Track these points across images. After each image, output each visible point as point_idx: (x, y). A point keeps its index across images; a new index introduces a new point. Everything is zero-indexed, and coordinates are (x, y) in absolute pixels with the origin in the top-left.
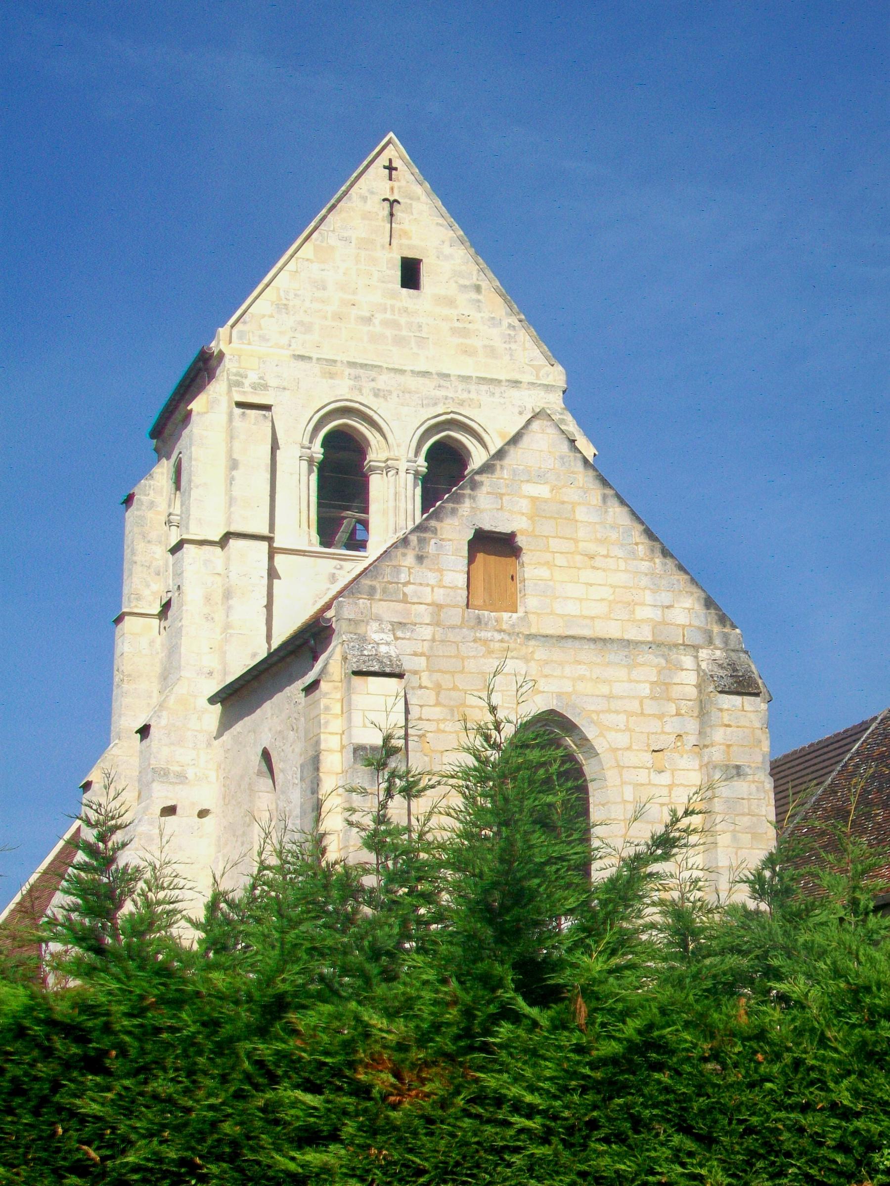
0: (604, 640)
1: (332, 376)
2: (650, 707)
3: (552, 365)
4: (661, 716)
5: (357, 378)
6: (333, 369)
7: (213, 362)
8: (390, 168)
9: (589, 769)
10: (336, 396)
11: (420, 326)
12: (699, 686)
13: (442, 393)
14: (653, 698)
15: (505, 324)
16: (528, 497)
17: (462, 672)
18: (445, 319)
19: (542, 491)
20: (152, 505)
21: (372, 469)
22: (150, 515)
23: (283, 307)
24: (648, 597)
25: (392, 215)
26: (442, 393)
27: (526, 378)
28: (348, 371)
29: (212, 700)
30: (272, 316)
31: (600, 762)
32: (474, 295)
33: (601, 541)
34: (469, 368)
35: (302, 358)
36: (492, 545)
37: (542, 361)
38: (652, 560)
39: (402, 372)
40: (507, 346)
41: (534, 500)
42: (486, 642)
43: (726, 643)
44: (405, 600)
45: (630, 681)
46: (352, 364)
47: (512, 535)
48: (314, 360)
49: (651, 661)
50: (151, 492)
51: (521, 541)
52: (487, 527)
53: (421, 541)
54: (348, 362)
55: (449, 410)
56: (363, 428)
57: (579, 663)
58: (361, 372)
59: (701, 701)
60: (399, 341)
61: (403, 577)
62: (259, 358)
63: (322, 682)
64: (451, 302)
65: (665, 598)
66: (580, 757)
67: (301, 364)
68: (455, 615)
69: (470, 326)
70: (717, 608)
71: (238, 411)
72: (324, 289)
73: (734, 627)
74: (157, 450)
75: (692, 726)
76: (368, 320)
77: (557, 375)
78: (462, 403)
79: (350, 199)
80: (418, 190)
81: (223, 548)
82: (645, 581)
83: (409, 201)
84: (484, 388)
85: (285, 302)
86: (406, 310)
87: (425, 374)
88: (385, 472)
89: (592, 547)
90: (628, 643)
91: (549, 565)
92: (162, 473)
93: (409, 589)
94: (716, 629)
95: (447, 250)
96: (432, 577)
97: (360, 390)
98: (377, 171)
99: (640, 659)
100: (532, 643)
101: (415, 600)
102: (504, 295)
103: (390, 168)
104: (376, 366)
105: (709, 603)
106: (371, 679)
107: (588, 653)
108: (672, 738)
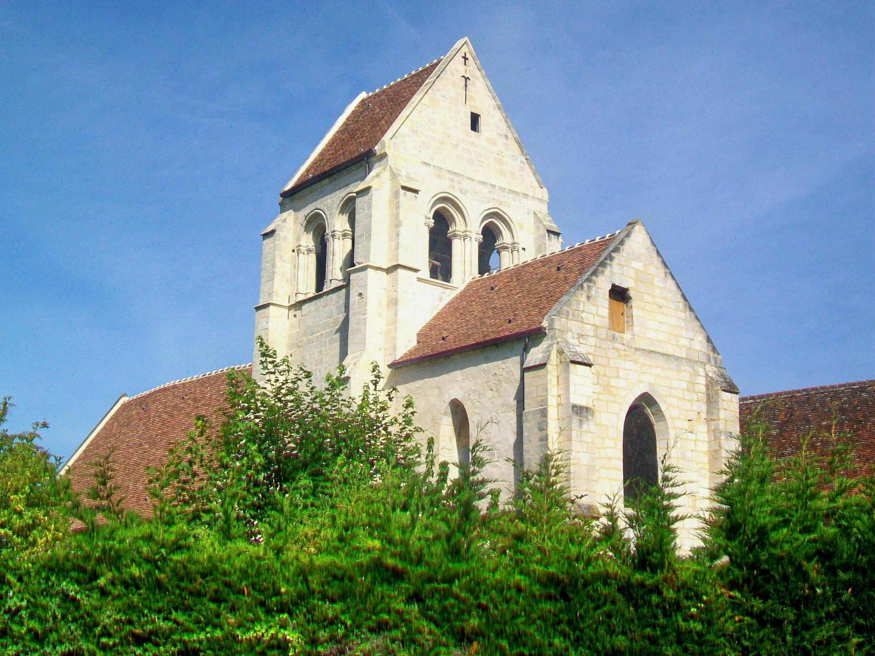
0: (667, 355)
2: (687, 396)
4: (691, 401)
7: (374, 159)
8: (465, 58)
9: (658, 427)
12: (707, 386)
13: (491, 196)
14: (688, 390)
17: (608, 366)
19: (638, 265)
20: (285, 238)
21: (455, 236)
23: (415, 131)
24: (684, 333)
25: (466, 86)
26: (491, 196)
27: (530, 193)
28: (448, 175)
29: (390, 366)
31: (667, 424)
32: (504, 140)
33: (665, 298)
34: (501, 182)
35: (426, 164)
36: (619, 294)
37: (536, 185)
39: (473, 180)
41: (636, 270)
42: (618, 350)
43: (716, 363)
44: (582, 322)
45: (678, 379)
46: (450, 172)
47: (627, 290)
49: (686, 367)
51: (631, 293)
52: (617, 284)
53: (589, 287)
56: (452, 210)
57: (657, 366)
58: (454, 177)
59: (708, 394)
61: (581, 308)
63: (548, 365)
64: (494, 143)
65: (691, 334)
66: (652, 419)
67: (425, 167)
68: (603, 333)
70: (712, 343)
71: (402, 191)
73: (718, 354)
74: (281, 204)
75: (704, 408)
76: (455, 146)
77: (544, 194)
78: (501, 204)
81: (387, 273)
82: (682, 324)
84: (511, 196)
86: (473, 144)
87: (484, 183)
89: (661, 301)
90: (678, 358)
91: (643, 309)
93: (584, 315)
94: (712, 354)
96: (593, 309)
98: (458, 59)
99: (682, 368)
100: (638, 353)
103: (465, 58)
105: (709, 340)
106: (578, 366)
107: (661, 361)
108: (696, 413)
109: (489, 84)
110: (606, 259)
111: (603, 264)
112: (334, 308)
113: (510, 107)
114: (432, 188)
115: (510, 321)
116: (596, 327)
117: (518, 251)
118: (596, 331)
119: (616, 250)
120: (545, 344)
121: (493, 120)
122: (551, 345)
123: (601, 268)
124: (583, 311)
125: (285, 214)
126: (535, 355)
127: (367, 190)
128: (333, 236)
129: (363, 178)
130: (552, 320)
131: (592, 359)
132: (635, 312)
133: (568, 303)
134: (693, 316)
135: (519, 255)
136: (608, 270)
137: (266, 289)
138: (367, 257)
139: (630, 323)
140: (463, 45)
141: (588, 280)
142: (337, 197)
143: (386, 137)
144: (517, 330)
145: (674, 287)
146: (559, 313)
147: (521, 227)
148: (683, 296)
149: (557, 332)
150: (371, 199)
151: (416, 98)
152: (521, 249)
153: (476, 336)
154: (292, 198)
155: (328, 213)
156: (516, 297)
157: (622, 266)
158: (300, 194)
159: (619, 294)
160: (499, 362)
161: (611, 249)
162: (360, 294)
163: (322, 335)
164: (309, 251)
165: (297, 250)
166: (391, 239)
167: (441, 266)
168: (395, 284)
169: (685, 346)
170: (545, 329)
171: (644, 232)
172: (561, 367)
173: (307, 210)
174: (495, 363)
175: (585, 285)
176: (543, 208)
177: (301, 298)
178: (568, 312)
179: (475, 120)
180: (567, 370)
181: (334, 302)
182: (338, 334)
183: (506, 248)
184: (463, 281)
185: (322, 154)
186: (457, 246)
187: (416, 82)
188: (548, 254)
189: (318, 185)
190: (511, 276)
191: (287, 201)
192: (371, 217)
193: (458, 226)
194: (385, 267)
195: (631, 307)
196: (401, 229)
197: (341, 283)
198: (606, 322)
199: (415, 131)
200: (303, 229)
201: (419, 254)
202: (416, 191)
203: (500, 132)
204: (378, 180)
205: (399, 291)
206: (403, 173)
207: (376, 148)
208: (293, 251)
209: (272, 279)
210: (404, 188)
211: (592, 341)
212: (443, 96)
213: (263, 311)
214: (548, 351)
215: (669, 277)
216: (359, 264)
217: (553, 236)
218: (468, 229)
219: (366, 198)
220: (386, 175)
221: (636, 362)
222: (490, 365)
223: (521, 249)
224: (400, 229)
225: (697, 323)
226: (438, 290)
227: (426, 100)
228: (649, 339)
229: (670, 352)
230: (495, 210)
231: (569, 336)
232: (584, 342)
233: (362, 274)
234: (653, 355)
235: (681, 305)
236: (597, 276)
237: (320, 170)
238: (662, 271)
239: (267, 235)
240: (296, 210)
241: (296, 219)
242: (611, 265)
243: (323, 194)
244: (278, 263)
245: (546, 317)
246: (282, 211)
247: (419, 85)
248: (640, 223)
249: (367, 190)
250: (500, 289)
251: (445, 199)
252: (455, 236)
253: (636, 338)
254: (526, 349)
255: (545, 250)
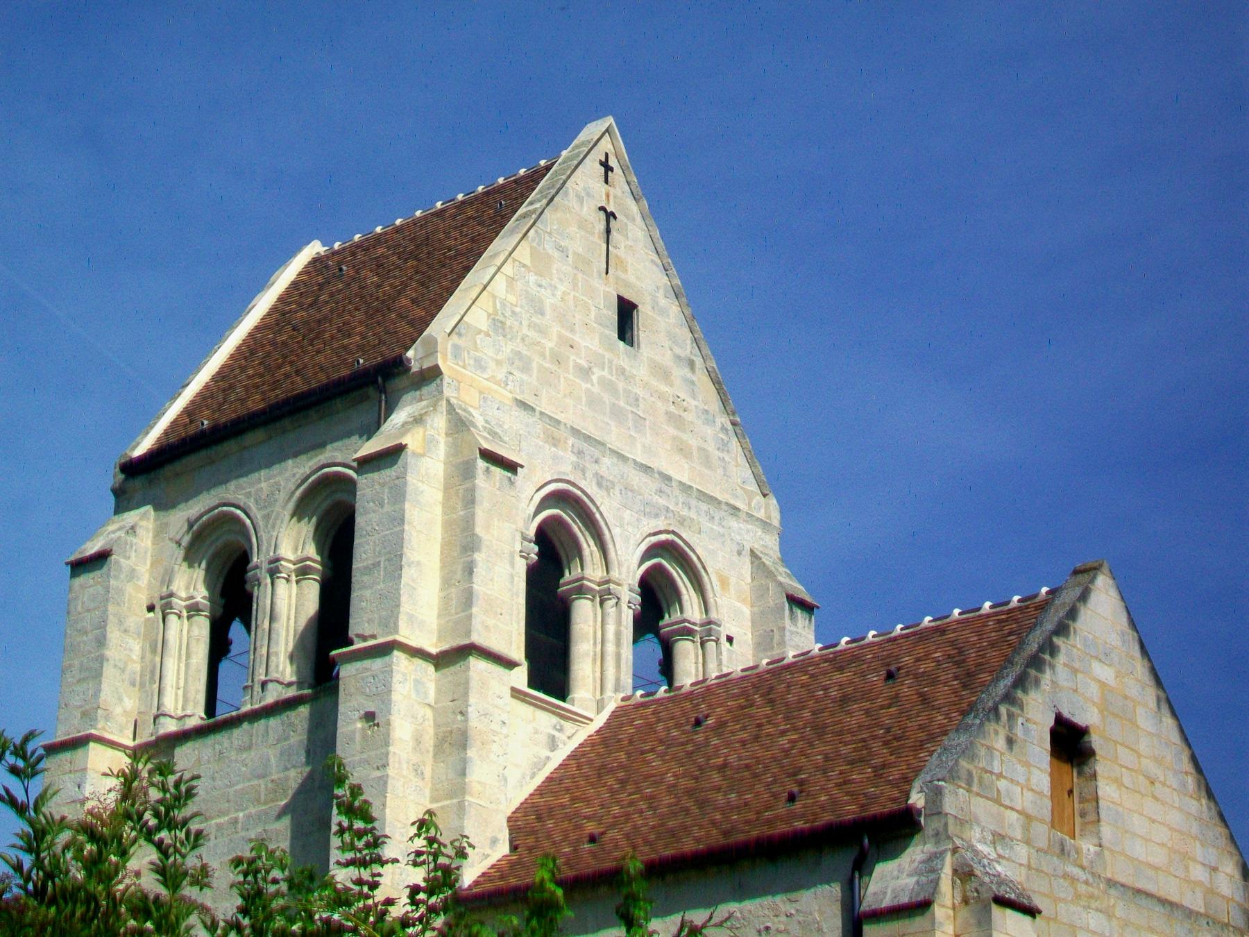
0: (1172, 904)
1: (555, 442)
3: (765, 496)
5: (580, 453)
6: (556, 433)
7: (400, 382)
10: (560, 473)
11: (637, 400)
13: (662, 501)
15: (719, 425)
16: (1100, 681)
18: (661, 396)
21: (581, 590)
22: (129, 589)
24: (1198, 851)
25: (608, 231)
26: (662, 501)
28: (571, 441)
30: (488, 335)
32: (686, 371)
33: (1158, 760)
34: (681, 472)
35: (523, 405)
37: (753, 487)
38: (1199, 800)
39: (623, 458)
40: (721, 455)
41: (1103, 685)
42: (1073, 880)
44: (998, 801)
46: (575, 432)
48: (537, 413)
50: (133, 554)
52: (1066, 714)
53: (1011, 716)
54: (572, 428)
55: (671, 529)
56: (577, 528)
58: (584, 446)
60: (617, 413)
62: (481, 393)
64: (665, 375)
65: (1212, 855)
68: (1041, 832)
69: (684, 415)
71: (481, 464)
72: (543, 314)
77: (770, 509)
78: (682, 521)
79: (566, 194)
80: (633, 207)
81: (437, 667)
82: (1195, 829)
83: (625, 220)
84: (704, 507)
85: (501, 318)
87: (646, 469)
88: (598, 599)
92: (147, 530)
93: (1002, 784)
95: (663, 302)
96: (1020, 772)
97: (583, 471)
100: (1112, 891)
101: (1007, 803)
102: (719, 383)
104: (599, 443)
109: (657, 234)
110: (1041, 649)
111: (1036, 662)
112: (273, 755)
113: (695, 294)
114: (544, 468)
115: (792, 798)
116: (1027, 817)
117: (717, 641)
118: (1026, 829)
119: (1062, 629)
120: (915, 853)
121: (663, 319)
122: (938, 856)
123: (1033, 672)
124: (1000, 776)
125: (131, 517)
126: (890, 880)
127: (394, 454)
128: (274, 573)
129: (370, 430)
130: (938, 792)
131: (1038, 902)
132: (1106, 789)
133: (968, 752)
134: (1214, 812)
135: (719, 653)
136: (1046, 677)
137: (76, 701)
138: (391, 621)
139: (1091, 817)
140: (600, 135)
141: (1008, 698)
142: (293, 474)
143: (439, 326)
144: (827, 818)
145: (1175, 737)
146: (952, 775)
147: (724, 582)
148: (1194, 759)
149: (951, 821)
150: (402, 476)
151: (501, 245)
152: (723, 639)
153: (697, 833)
154: (144, 478)
155: (258, 515)
156: (784, 741)
157: (1075, 671)
158: (177, 466)
159: (1070, 743)
160: (779, 899)
161: (1049, 626)
162: (370, 717)
163: (236, 821)
164: (194, 609)
165: (162, 606)
166: (446, 582)
167: (549, 667)
168: (458, 700)
169: (1200, 883)
170: (919, 812)
171: (1113, 593)
172: (964, 913)
173: (196, 508)
174: (767, 900)
175: (1003, 709)
176: (769, 545)
177: (170, 726)
178: (970, 774)
179: (626, 312)
180: (985, 922)
181: (271, 740)
182: (286, 821)
183: (690, 632)
184: (600, 706)
185: (222, 375)
186: (584, 615)
187: (490, 213)
188: (791, 655)
189: (231, 445)
190: (744, 693)
191: (138, 482)
192: (402, 521)
193: (591, 569)
194: (434, 650)
195: (1094, 776)
196: (479, 557)
197: (292, 692)
198: (1046, 813)
199: (498, 325)
200: (181, 553)
201: (505, 624)
202: (511, 467)
203: (678, 351)
204: (414, 426)
205: (472, 711)
206: (479, 421)
207: (410, 354)
208: (151, 608)
209: (97, 675)
210: (489, 456)
211: (1022, 852)
212: (562, 249)
213: (66, 756)
214: (931, 866)
215: (1165, 710)
216: (364, 638)
217: (798, 612)
218: (615, 574)
219: (388, 474)
220: (439, 422)
221: (1109, 914)
222: (749, 905)
223: (723, 639)
224: (477, 556)
225: (1220, 830)
226: (546, 721)
227: (523, 253)
228: (1132, 859)
229: (1175, 898)
230: (670, 537)
231: (975, 834)
232: (1006, 853)
233: (377, 664)
234: (1144, 901)
235: (1191, 781)
236: (1025, 691)
237: (229, 414)
238: (1151, 694)
239: (81, 566)
240: (162, 505)
241: (160, 531)
242: (1052, 667)
243: (244, 468)
244: (113, 634)
245: (917, 784)
246: (119, 510)
247: (497, 222)
248: (1105, 569)
249: (394, 454)
250: (721, 724)
251: (560, 498)
252: (581, 590)
253: (1106, 853)
254: (862, 866)
255: (782, 643)
